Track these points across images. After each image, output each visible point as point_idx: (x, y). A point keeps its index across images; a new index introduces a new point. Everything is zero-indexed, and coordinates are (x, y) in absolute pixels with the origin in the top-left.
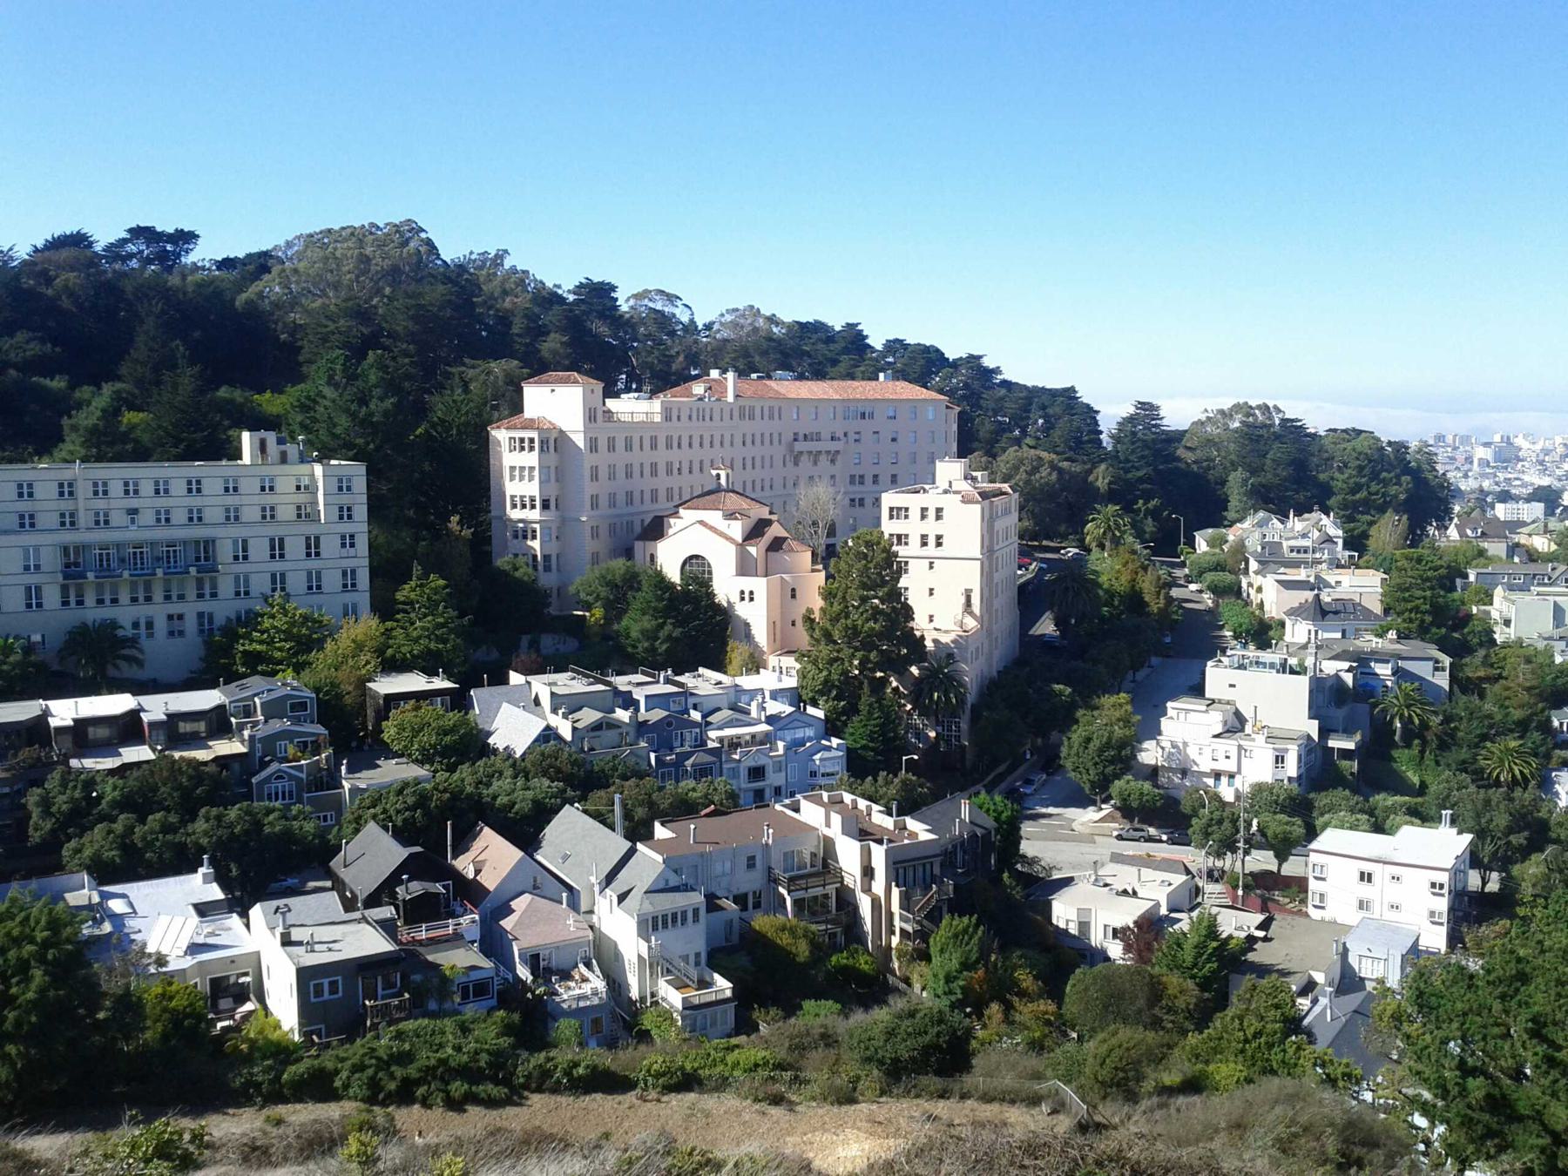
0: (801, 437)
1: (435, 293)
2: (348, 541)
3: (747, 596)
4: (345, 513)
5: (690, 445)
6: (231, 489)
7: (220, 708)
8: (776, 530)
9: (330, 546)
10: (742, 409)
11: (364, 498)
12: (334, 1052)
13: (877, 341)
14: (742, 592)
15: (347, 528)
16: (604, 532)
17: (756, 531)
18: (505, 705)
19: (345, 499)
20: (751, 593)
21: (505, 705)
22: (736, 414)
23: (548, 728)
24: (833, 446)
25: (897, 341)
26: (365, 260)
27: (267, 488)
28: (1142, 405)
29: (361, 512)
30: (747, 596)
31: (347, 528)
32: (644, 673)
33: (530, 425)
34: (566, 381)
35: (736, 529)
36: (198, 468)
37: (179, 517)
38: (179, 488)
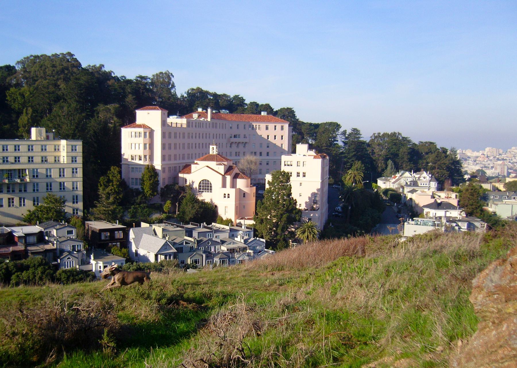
0: (233, 136)
1: (83, 79)
2: (74, 171)
3: (227, 196)
4: (74, 160)
5: (196, 138)
6: (30, 148)
7: (41, 232)
8: (236, 171)
9: (68, 173)
10: (213, 123)
11: (81, 154)
12: (492, 277)
13: (247, 102)
14: (225, 194)
15: (74, 166)
16: (167, 170)
17: (228, 170)
18: (144, 234)
19: (74, 154)
20: (229, 195)
21: (144, 234)
22: (211, 125)
23: (199, 233)
24: (245, 140)
25: (254, 102)
26: (54, 66)
27: (43, 149)
28: (354, 130)
29: (80, 160)
30: (227, 196)
31: (74, 166)
32: (192, 224)
33: (140, 126)
34: (154, 109)
35: (221, 169)
36: (17, 142)
37: (11, 159)
38: (11, 148)
